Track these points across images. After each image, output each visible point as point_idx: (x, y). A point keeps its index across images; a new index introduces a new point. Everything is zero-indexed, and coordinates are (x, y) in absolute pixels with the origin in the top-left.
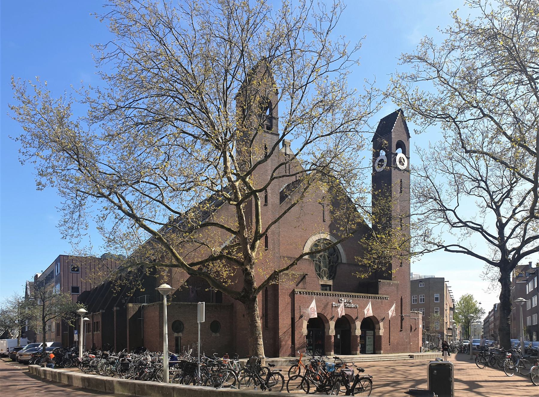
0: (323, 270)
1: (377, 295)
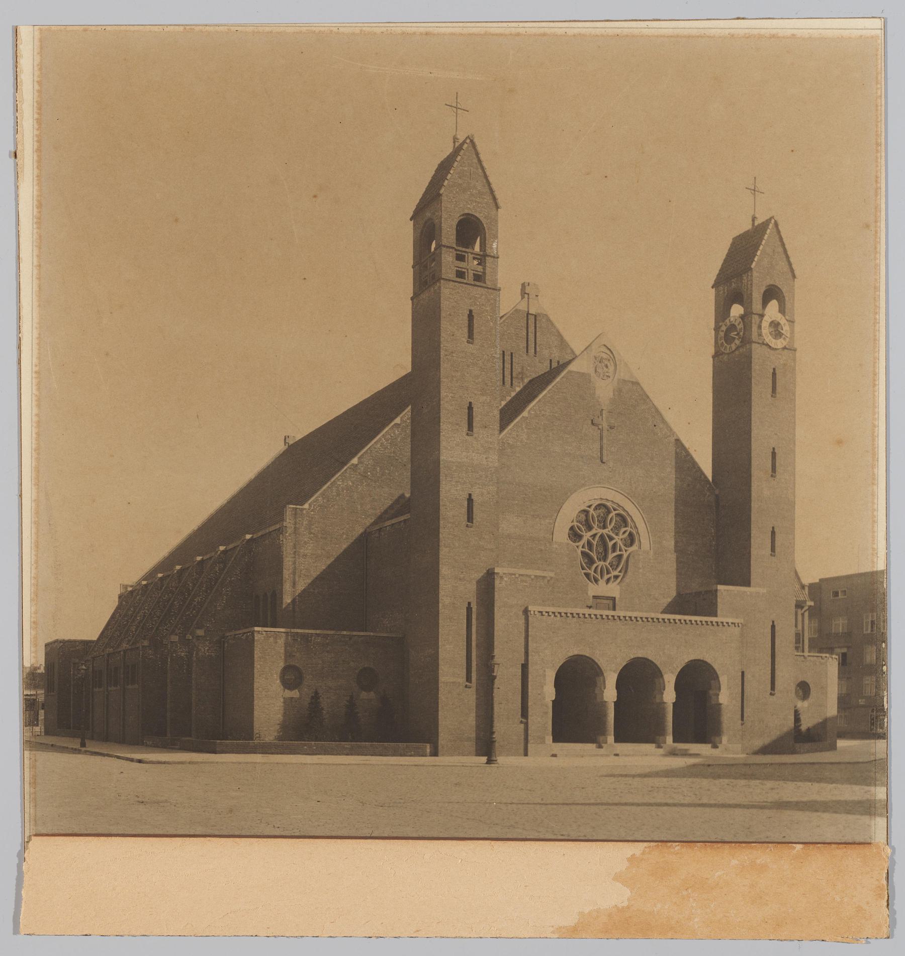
1: (714, 619)
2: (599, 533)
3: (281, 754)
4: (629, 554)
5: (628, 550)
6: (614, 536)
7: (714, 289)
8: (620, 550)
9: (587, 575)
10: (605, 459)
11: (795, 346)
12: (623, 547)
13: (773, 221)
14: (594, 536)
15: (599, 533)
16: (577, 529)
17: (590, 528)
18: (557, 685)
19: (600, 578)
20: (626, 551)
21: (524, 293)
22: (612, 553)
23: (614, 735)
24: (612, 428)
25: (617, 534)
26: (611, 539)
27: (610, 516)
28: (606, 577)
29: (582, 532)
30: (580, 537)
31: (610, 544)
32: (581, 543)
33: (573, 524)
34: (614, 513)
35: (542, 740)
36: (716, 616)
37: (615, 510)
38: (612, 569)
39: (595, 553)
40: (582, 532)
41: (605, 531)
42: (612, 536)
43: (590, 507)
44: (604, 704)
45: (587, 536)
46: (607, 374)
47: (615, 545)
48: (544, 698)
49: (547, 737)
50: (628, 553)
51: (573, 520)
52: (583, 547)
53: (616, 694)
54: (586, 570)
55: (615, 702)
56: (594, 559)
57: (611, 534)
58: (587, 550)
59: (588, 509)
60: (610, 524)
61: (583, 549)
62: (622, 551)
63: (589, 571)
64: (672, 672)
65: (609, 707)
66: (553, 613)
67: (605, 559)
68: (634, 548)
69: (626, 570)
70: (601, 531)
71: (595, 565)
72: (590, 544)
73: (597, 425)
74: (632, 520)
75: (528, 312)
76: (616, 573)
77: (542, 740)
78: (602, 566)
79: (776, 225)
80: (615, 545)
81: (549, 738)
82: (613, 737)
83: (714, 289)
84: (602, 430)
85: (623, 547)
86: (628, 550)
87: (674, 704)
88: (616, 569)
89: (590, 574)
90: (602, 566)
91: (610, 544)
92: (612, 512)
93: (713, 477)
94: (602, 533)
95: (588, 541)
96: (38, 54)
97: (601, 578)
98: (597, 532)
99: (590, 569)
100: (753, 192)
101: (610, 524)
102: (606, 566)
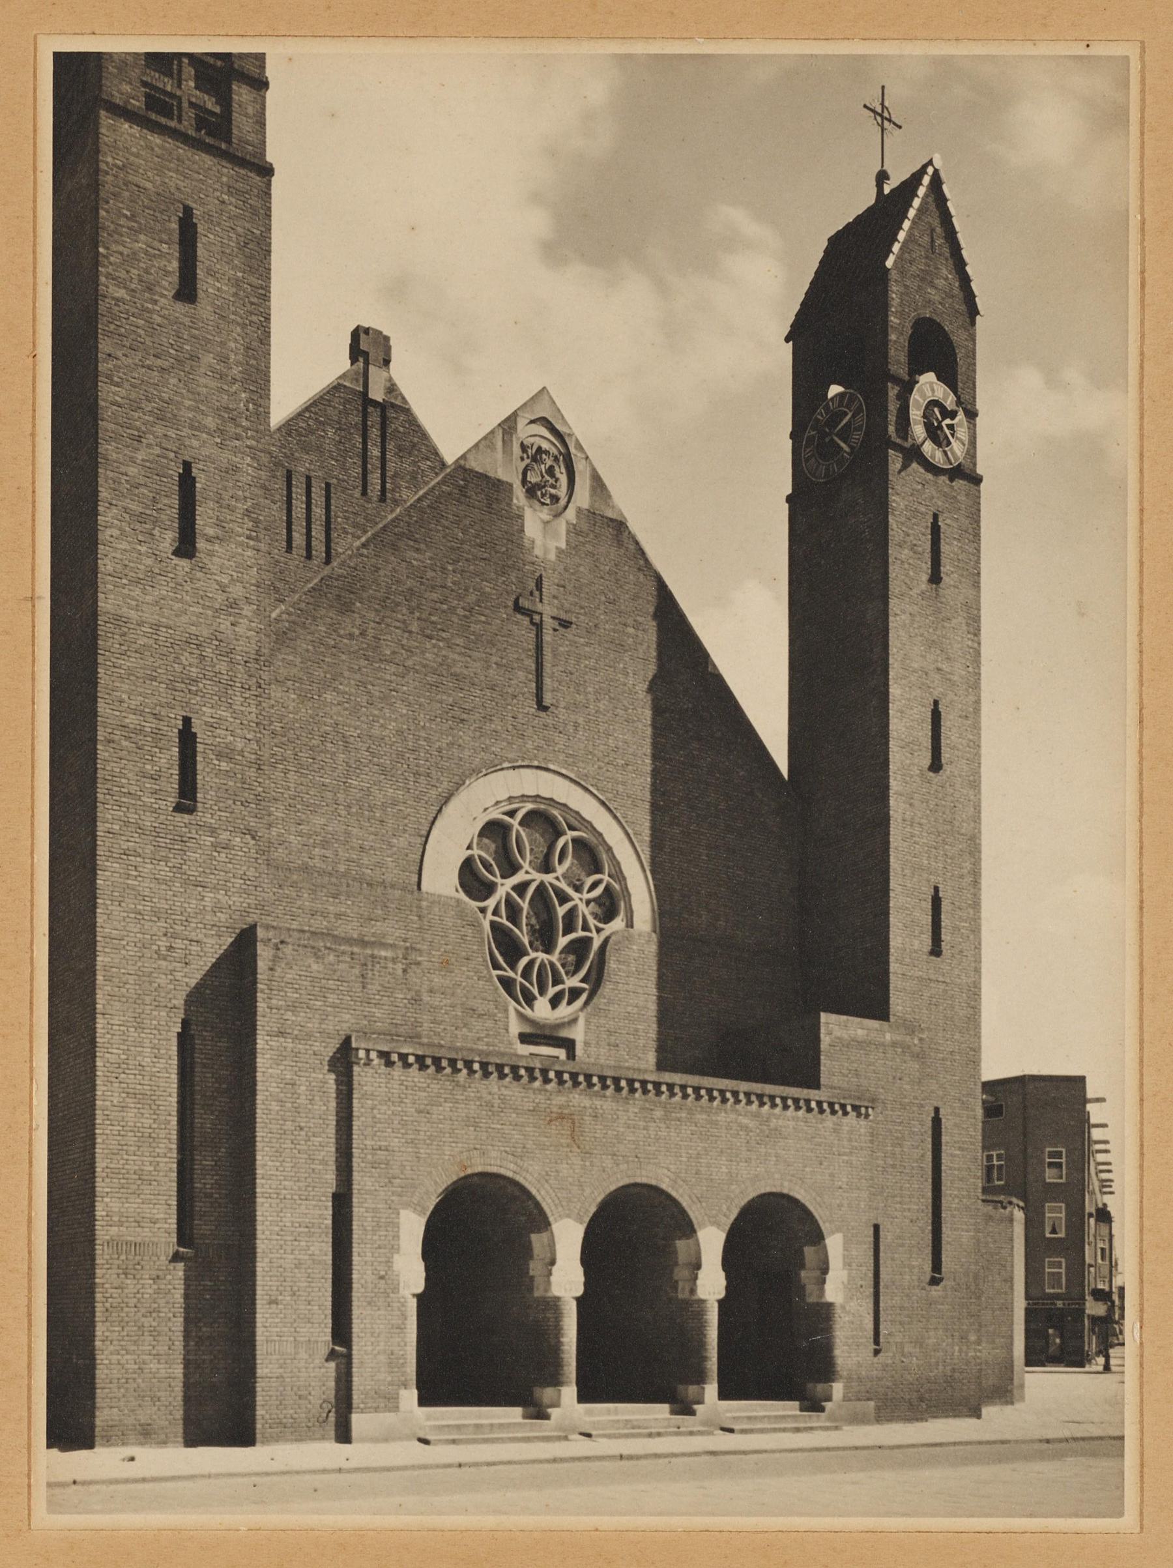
0: (531, 963)
1: (813, 1094)
2: (534, 880)
3: (976, 883)
4: (606, 941)
5: (603, 929)
6: (570, 891)
7: (791, 343)
8: (586, 928)
9: (507, 984)
10: (548, 699)
11: (979, 471)
12: (592, 922)
13: (930, 170)
14: (521, 888)
15: (534, 880)
16: (481, 866)
17: (511, 868)
18: (431, 1249)
19: (535, 991)
20: (599, 930)
21: (356, 352)
22: (564, 935)
23: (578, 1384)
24: (566, 624)
25: (578, 889)
26: (564, 898)
27: (561, 842)
28: (552, 991)
29: (494, 875)
30: (488, 889)
31: (561, 911)
32: (491, 903)
33: (470, 852)
34: (571, 834)
35: (391, 1403)
36: (817, 1086)
37: (571, 828)
38: (567, 973)
39: (524, 928)
40: (494, 875)
41: (548, 878)
42: (567, 894)
43: (512, 814)
44: (553, 1305)
45: (505, 887)
46: (553, 491)
47: (571, 915)
48: (396, 1289)
49: (403, 1393)
50: (603, 935)
51: (471, 842)
52: (496, 912)
53: (582, 1279)
54: (505, 970)
55: (578, 1299)
56: (525, 945)
57: (563, 885)
58: (504, 921)
59: (506, 818)
60: (560, 862)
61: (496, 919)
62: (589, 930)
63: (511, 974)
64: (718, 1224)
65: (565, 1311)
66: (667, 1084)
67: (548, 948)
68: (618, 924)
69: (596, 978)
70: (539, 877)
71: (524, 961)
72: (513, 912)
73: (528, 613)
74: (613, 858)
75: (365, 393)
76: (574, 982)
77: (391, 1403)
78: (543, 960)
79: (937, 181)
80: (571, 915)
81: (410, 1396)
82: (575, 1388)
83: (791, 343)
84: (539, 627)
85: (592, 922)
86: (603, 929)
87: (721, 1303)
88: (575, 972)
89: (514, 980)
90: (542, 965)
91: (561, 911)
92: (563, 833)
93: (789, 776)
94: (542, 883)
95: (507, 901)
96: (39, 598)
97: (541, 994)
98: (528, 877)
99: (513, 967)
100: (879, 119)
101: (560, 862)
102: (552, 965)
